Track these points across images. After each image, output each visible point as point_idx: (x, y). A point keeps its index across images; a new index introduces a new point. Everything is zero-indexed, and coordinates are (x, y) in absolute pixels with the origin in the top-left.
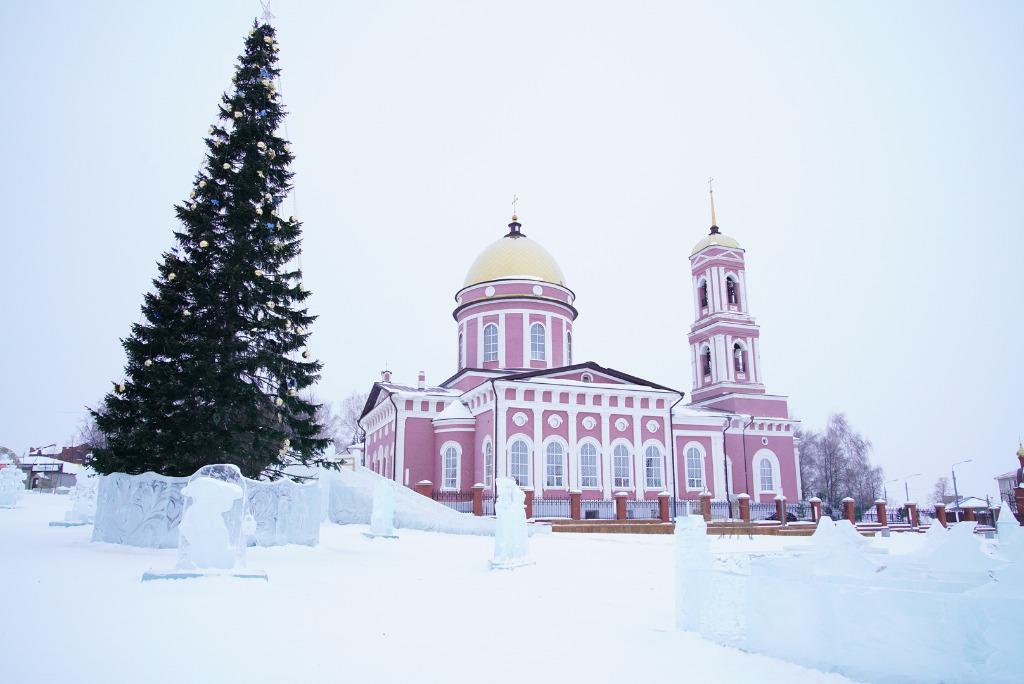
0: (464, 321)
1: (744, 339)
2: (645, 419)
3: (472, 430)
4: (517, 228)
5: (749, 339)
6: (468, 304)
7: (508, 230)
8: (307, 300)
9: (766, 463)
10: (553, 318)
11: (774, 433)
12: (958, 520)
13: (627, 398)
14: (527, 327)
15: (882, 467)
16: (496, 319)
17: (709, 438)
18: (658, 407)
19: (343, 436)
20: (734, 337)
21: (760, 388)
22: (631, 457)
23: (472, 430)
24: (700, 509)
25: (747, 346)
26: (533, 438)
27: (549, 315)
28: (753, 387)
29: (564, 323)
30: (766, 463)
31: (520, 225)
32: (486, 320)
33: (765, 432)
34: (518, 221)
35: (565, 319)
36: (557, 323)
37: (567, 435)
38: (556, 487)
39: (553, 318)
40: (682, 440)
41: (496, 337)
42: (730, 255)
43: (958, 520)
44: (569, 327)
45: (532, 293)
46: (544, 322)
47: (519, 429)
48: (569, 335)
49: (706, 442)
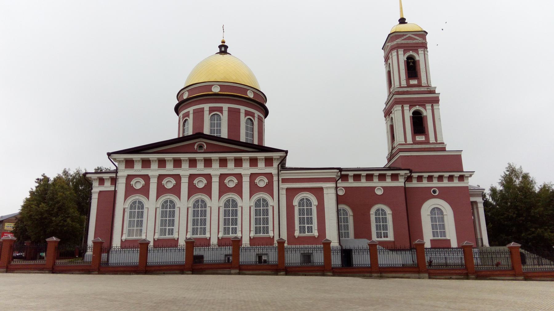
1: (424, 106)
2: (161, 177)
5: (429, 107)
6: (177, 109)
7: (218, 51)
9: (436, 211)
11: (446, 184)
14: (243, 119)
15: (29, 191)
17: (321, 189)
20: (411, 107)
21: (441, 146)
24: (405, 251)
25: (427, 112)
26: (241, 197)
28: (432, 146)
29: (256, 116)
30: (436, 212)
33: (435, 184)
35: (257, 113)
37: (211, 195)
38: (307, 234)
40: (291, 193)
41: (220, 130)
42: (409, 38)
47: (171, 191)
49: (319, 193)
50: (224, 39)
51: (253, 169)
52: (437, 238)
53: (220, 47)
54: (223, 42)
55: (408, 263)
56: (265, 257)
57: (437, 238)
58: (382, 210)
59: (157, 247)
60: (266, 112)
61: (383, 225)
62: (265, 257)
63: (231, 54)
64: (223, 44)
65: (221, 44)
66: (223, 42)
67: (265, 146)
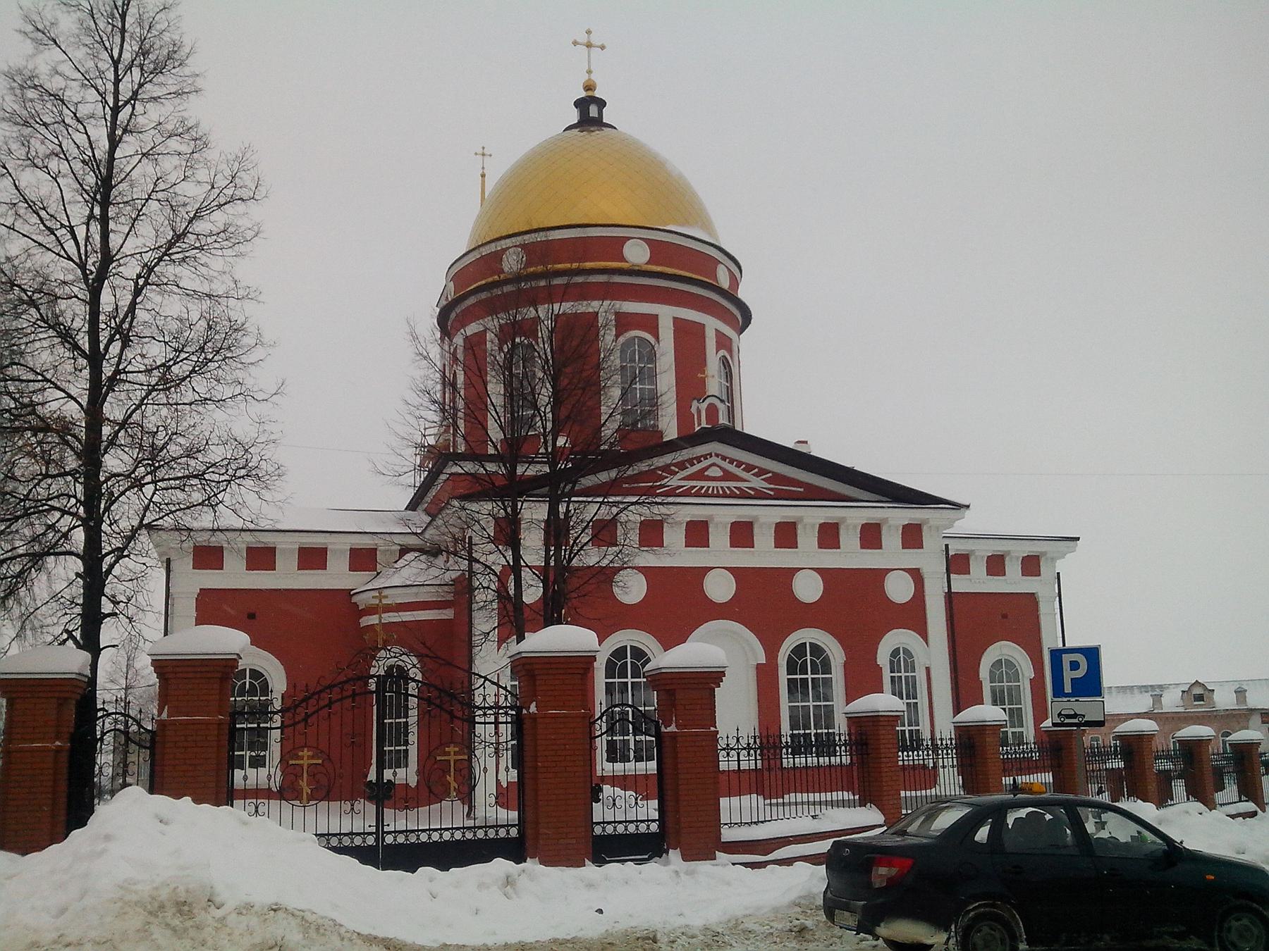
0: (459, 340)
3: (448, 614)
4: (593, 111)
7: (574, 116)
8: (17, 61)
10: (676, 321)
12: (790, 704)
13: (822, 526)
16: (529, 329)
18: (906, 545)
19: (615, 360)
22: (921, 676)
23: (448, 614)
26: (925, 636)
27: (666, 314)
31: (601, 104)
32: (506, 334)
34: (597, 94)
35: (712, 324)
36: (688, 336)
39: (676, 321)
43: (790, 704)
44: (724, 342)
45: (623, 259)
46: (655, 332)
48: (725, 363)
50: (593, 77)
51: (193, 651)
52: (413, 738)
53: (579, 104)
54: (589, 87)
55: (1039, 774)
56: (245, 778)
57: (413, 738)
58: (817, 650)
59: (1022, 760)
60: (744, 318)
61: (907, 677)
62: (245, 778)
63: (615, 128)
64: (590, 93)
65: (583, 94)
66: (589, 87)
67: (748, 430)
